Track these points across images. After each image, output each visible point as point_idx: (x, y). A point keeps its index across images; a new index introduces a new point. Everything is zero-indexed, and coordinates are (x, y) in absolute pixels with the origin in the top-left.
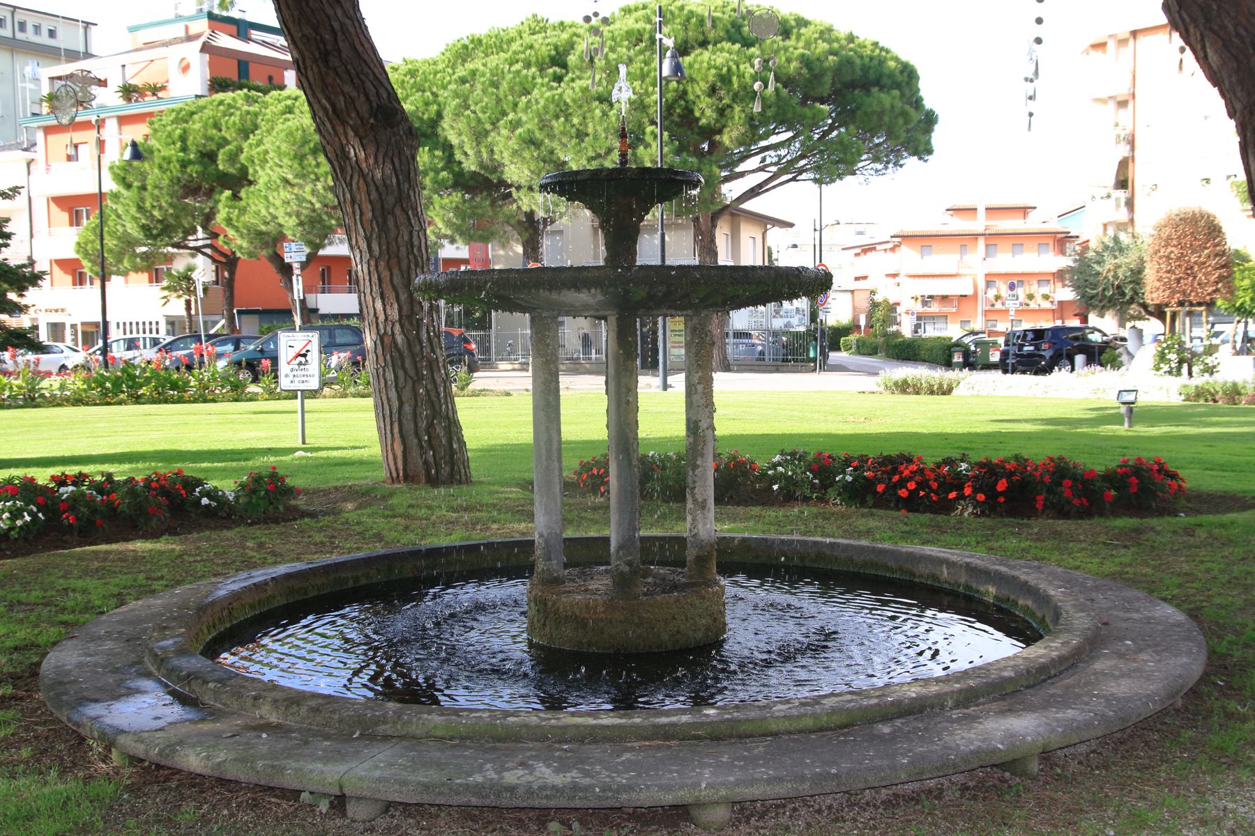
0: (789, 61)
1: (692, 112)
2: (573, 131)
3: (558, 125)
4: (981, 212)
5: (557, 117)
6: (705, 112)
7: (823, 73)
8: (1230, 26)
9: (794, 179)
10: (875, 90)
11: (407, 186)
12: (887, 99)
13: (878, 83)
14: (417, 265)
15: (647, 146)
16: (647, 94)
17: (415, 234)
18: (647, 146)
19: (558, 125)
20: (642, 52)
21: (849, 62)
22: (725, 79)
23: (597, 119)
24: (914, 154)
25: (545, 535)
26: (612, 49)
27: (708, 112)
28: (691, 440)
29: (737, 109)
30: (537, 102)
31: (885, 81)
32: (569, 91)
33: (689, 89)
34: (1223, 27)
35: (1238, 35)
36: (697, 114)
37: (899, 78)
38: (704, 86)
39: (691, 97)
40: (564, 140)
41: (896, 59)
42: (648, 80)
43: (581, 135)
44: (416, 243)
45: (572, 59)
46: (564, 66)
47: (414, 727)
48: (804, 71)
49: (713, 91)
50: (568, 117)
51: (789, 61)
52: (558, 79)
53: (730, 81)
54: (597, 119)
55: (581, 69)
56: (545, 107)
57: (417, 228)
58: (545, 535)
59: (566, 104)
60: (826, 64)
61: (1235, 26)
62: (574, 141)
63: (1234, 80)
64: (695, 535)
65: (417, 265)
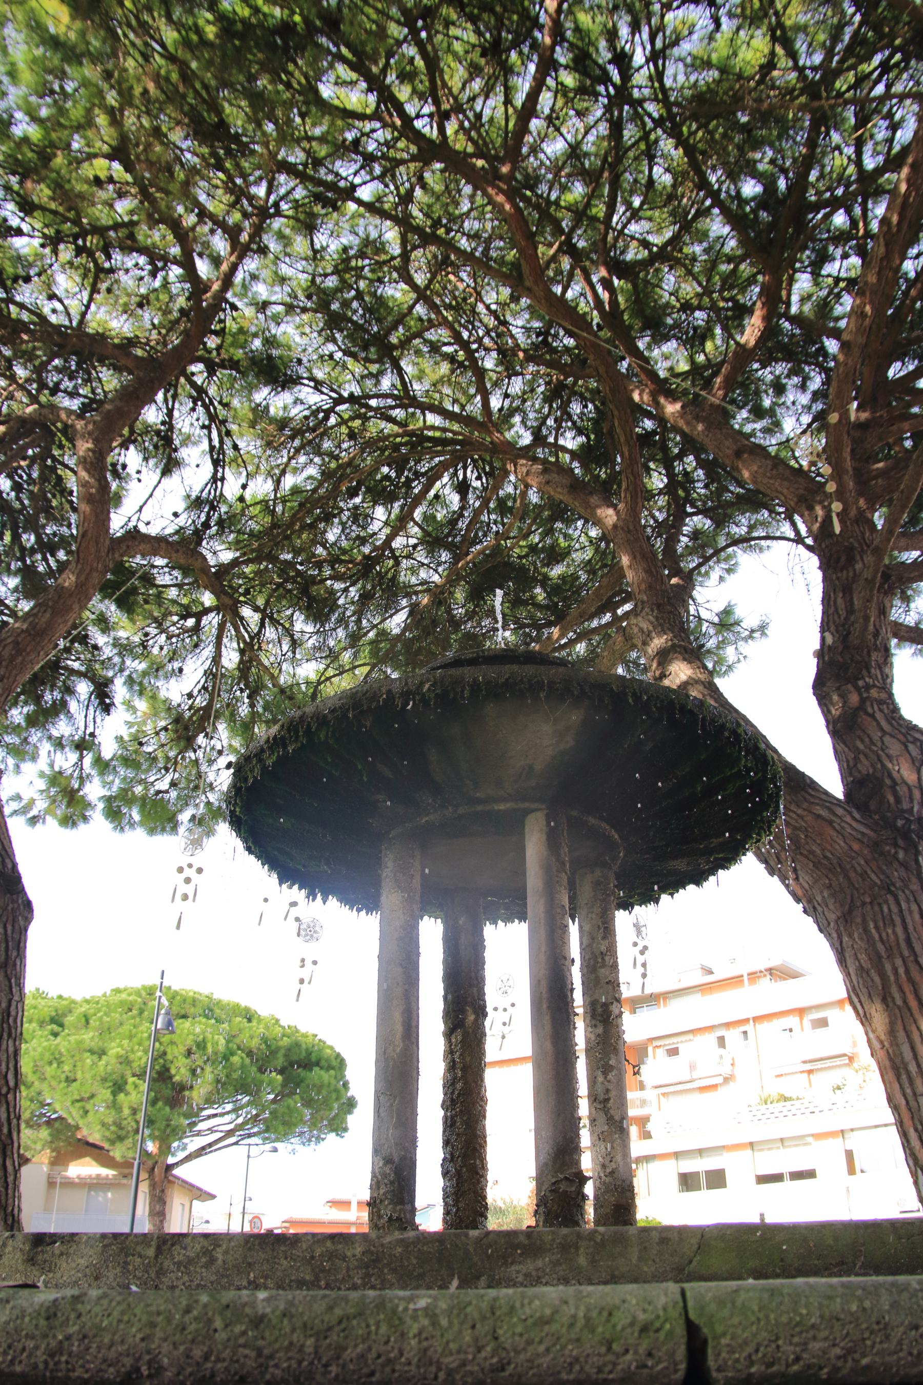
0: (252, 1037)
1: (168, 1070)
2: (63, 1076)
3: (50, 1071)
4: (354, 1205)
5: (50, 1063)
6: (180, 1071)
7: (278, 1049)
8: (818, 852)
9: (236, 1143)
10: (316, 1069)
11: (15, 954)
12: (326, 1076)
13: (317, 1064)
14: (10, 1035)
15: (127, 1094)
16: (133, 1051)
17: (14, 1003)
18: (127, 1094)
19: (50, 1071)
20: (133, 1017)
21: (297, 1044)
22: (201, 1045)
23: (87, 1067)
24: (332, 1130)
25: (396, 1160)
26: (106, 1014)
27: (183, 1071)
28: (600, 1030)
29: (208, 1069)
30: (34, 1050)
31: (323, 1063)
32: (62, 1044)
33: (169, 1050)
34: (811, 852)
35: (825, 857)
36: (173, 1071)
37: (334, 1063)
38: (182, 1049)
39: (169, 1057)
40: (54, 1083)
41: (331, 1048)
42: (135, 1040)
43: (70, 1080)
44: (13, 1013)
45: (69, 1020)
46: (62, 1025)
47: (634, 1256)
48: (263, 1046)
49: (189, 1053)
50: (60, 1063)
51: (252, 1037)
52: (55, 1035)
53: (205, 1048)
54: (87, 1067)
55: (76, 1028)
56: (42, 1055)
57: (16, 998)
58: (396, 1160)
59: (61, 1054)
60: (281, 1043)
61: (823, 850)
62: (63, 1084)
63: (826, 894)
64: (612, 1173)
65: (10, 1035)
